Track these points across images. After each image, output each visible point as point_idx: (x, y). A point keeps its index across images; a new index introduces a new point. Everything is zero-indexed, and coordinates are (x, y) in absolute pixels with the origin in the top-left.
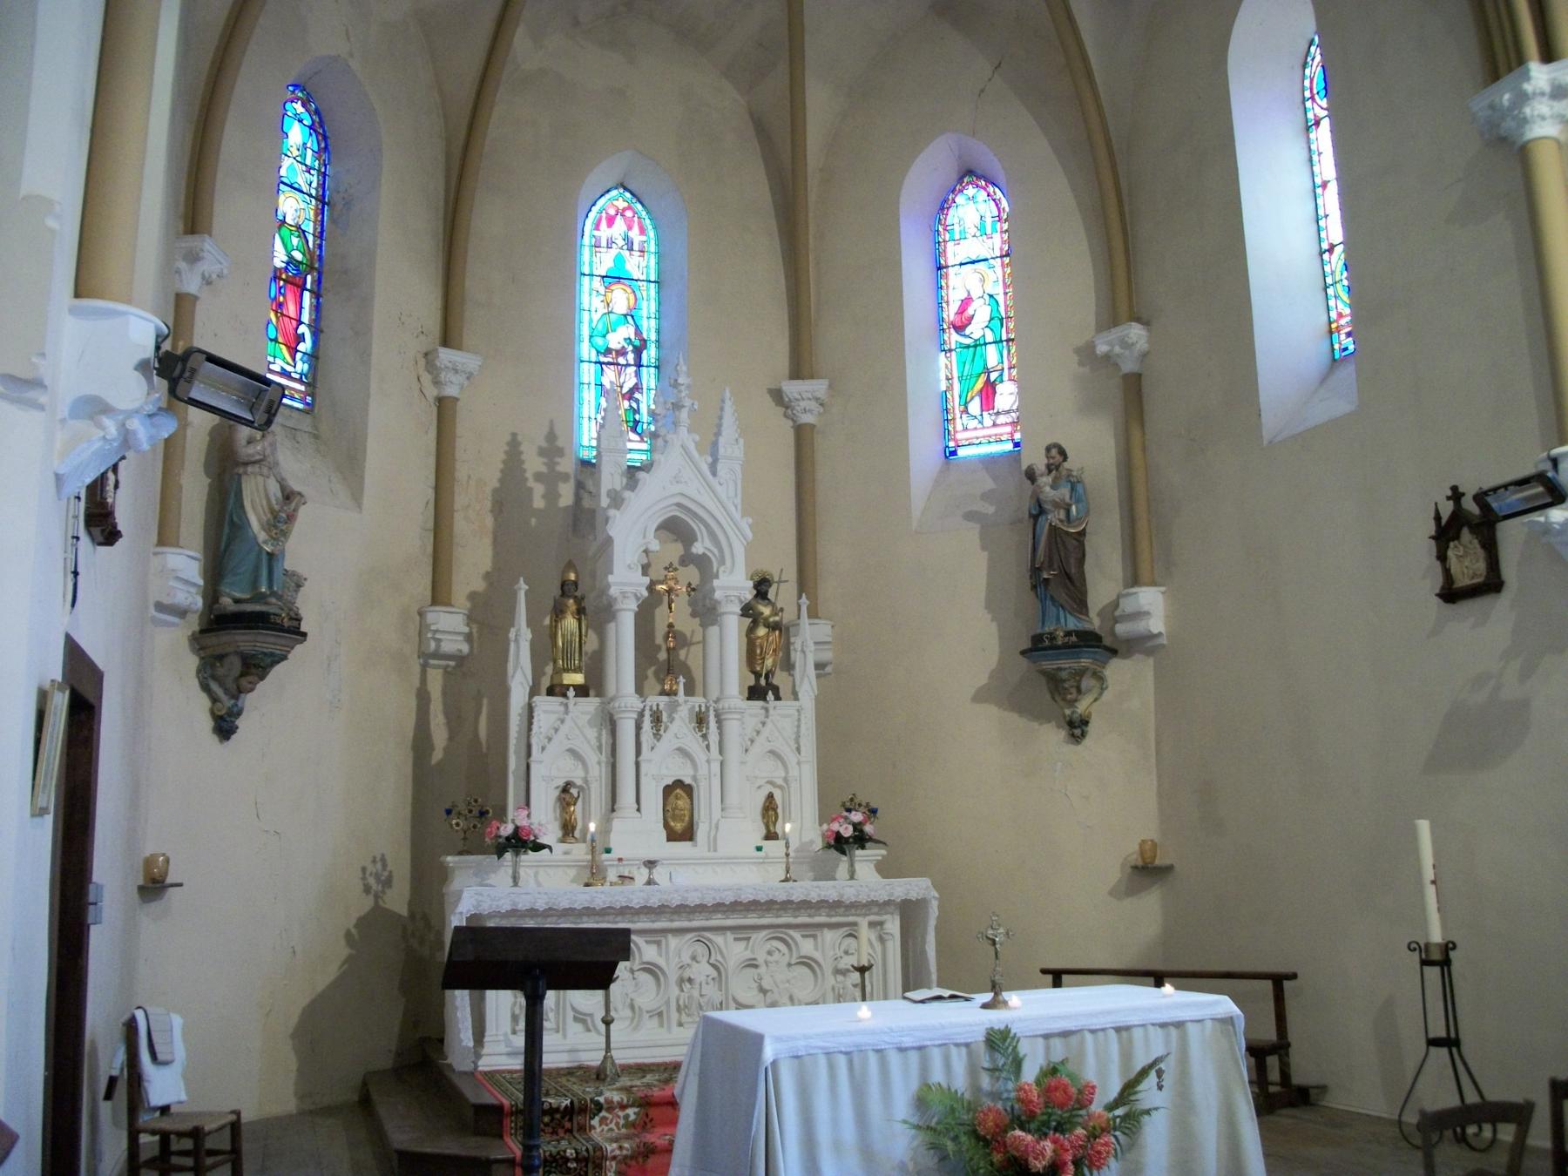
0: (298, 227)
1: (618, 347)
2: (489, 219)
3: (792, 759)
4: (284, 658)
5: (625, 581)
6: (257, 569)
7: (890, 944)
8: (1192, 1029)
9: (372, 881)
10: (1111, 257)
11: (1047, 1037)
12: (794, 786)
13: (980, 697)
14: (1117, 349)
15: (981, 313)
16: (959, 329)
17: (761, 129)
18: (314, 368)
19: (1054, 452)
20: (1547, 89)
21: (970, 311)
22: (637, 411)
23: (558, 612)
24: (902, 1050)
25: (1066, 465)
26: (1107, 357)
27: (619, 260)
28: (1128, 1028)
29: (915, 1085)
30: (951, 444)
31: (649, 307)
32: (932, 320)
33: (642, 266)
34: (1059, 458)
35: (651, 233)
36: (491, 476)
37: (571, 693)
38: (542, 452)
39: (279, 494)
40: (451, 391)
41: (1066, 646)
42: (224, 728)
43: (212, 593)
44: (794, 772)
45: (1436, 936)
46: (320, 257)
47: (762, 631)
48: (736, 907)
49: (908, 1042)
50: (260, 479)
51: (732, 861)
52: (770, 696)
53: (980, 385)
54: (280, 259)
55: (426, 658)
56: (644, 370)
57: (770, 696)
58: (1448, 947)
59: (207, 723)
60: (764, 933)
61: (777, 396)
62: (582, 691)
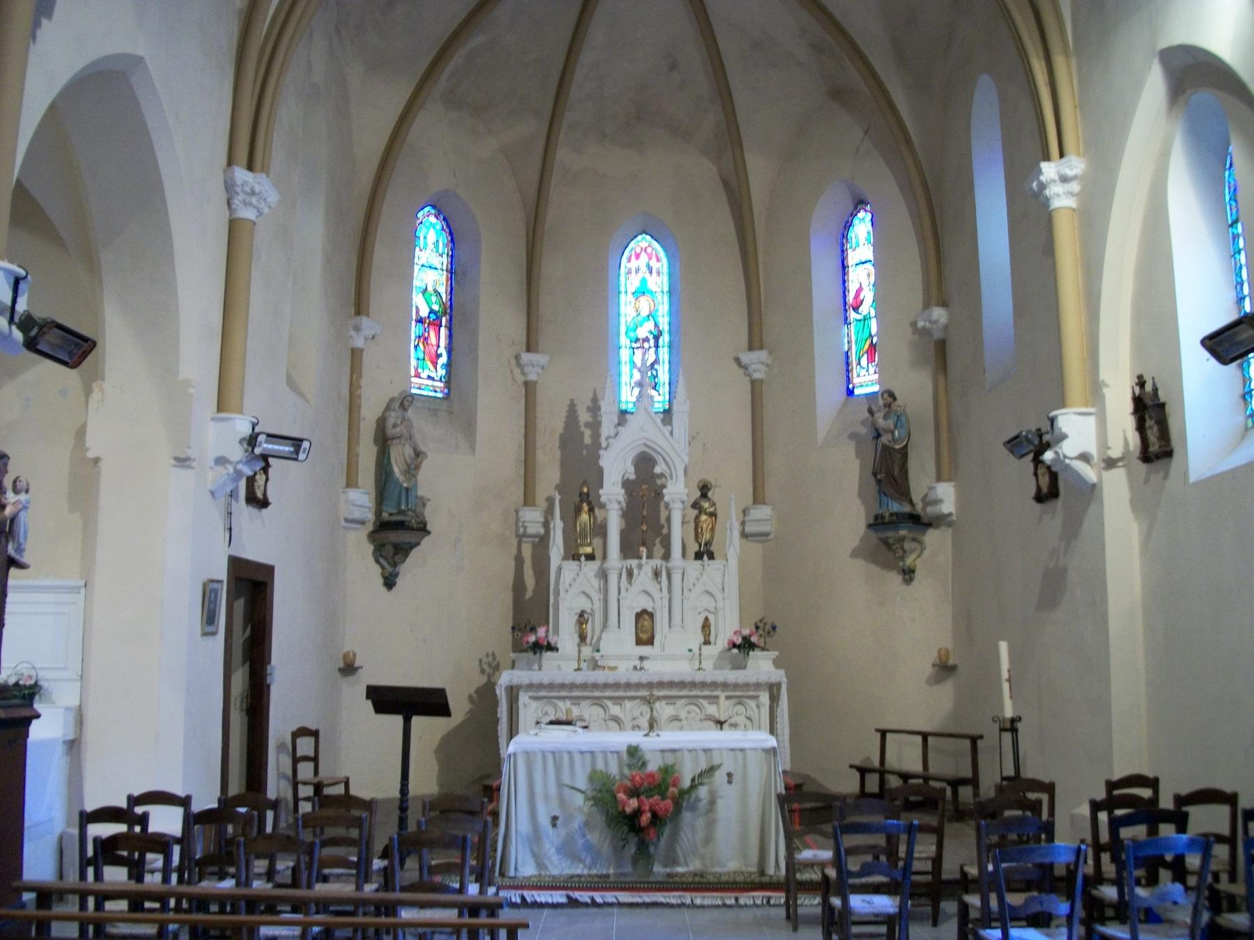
2: (553, 268)
3: (719, 595)
5: (612, 493)
6: (400, 497)
7: (762, 710)
8: (750, 754)
9: (485, 667)
10: (20, 587)
11: (662, 751)
12: (721, 613)
13: (855, 554)
14: (928, 324)
16: (856, 309)
17: (726, 184)
18: (449, 373)
19: (886, 396)
20: (1057, 178)
22: (656, 377)
23: (578, 511)
24: (582, 753)
25: (897, 403)
26: (924, 328)
27: (644, 281)
28: (710, 750)
29: (588, 769)
33: (659, 283)
34: (890, 400)
36: (559, 425)
37: (583, 558)
38: (589, 409)
39: (412, 454)
40: (532, 377)
41: (890, 523)
42: (389, 583)
43: (378, 512)
44: (720, 604)
45: (1009, 713)
47: (704, 517)
48: (671, 684)
49: (584, 748)
51: (673, 658)
52: (705, 557)
53: (867, 347)
54: (424, 313)
55: (520, 537)
56: (660, 350)
57: (705, 557)
58: (1013, 721)
59: (381, 581)
60: (683, 701)
62: (590, 557)
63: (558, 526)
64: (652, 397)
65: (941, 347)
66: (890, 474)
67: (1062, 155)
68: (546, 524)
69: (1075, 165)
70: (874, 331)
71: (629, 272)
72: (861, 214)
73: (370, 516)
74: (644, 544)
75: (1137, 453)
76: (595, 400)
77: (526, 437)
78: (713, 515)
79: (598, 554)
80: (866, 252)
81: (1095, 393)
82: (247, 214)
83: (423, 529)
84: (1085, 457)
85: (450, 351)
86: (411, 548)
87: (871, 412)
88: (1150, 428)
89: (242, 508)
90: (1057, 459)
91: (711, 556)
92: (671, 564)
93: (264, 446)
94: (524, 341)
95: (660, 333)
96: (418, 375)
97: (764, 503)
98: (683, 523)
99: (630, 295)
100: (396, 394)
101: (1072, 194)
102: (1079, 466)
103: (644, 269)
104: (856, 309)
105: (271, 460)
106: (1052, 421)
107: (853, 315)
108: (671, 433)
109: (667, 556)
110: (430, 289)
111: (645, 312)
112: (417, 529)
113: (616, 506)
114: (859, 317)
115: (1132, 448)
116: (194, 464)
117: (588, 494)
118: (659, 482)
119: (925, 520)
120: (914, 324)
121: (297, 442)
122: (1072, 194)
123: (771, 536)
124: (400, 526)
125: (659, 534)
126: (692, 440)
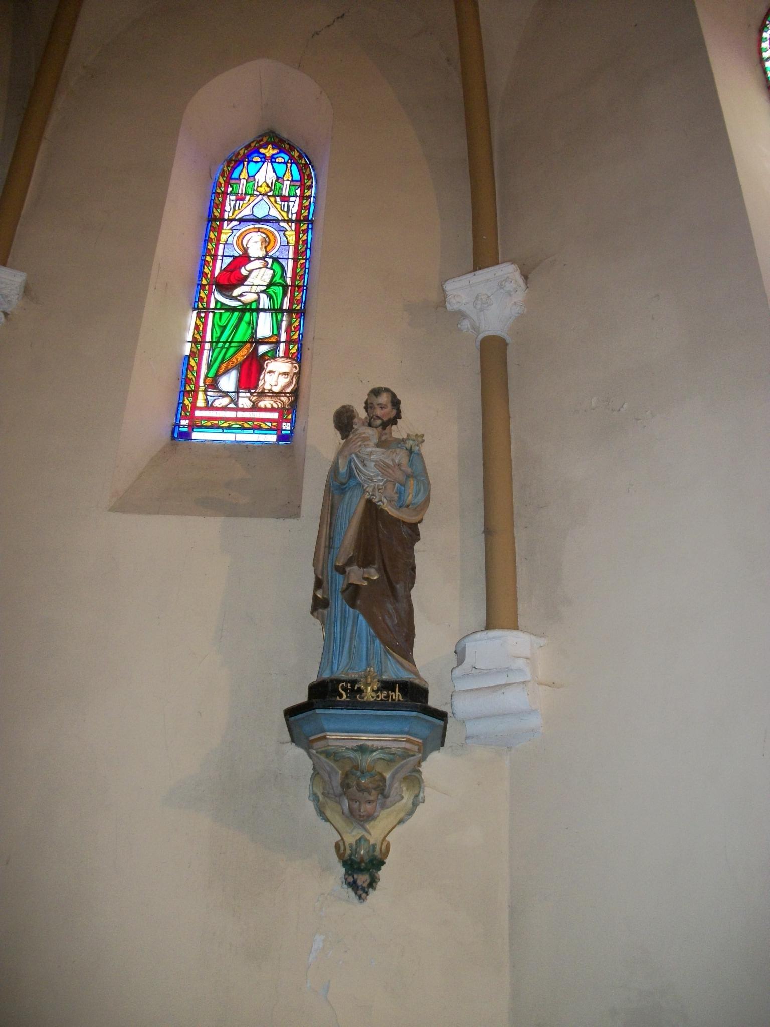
15: (258, 275)
19: (384, 399)
42: (362, 870)
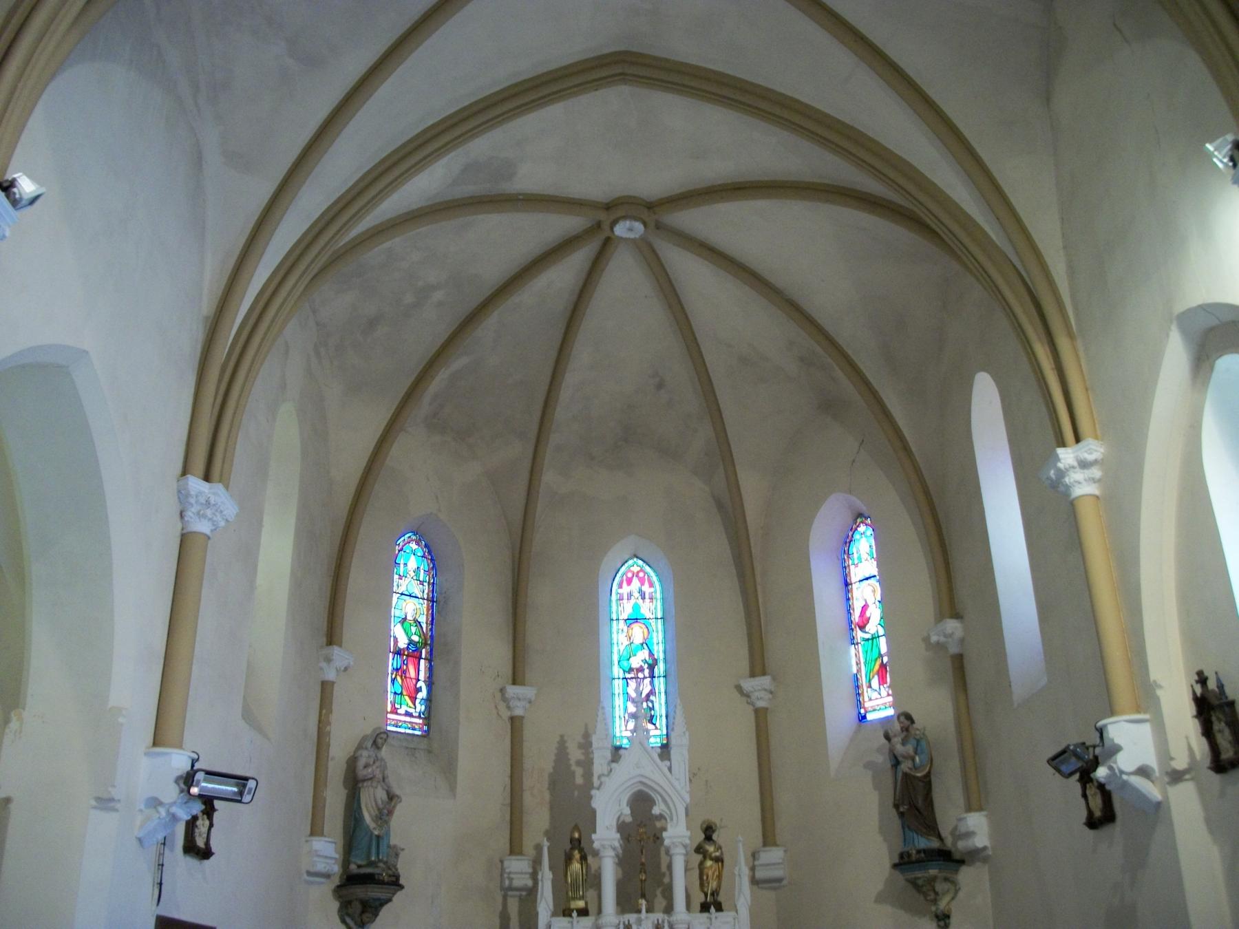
0: (416, 621)
1: (638, 666)
2: (541, 594)
4: (390, 900)
5: (606, 837)
13: (879, 899)
14: (942, 639)
16: (862, 628)
17: (720, 506)
19: (902, 718)
20: (1075, 464)
21: (868, 614)
22: (653, 708)
23: (569, 859)
26: (938, 643)
27: (636, 607)
30: (862, 711)
31: (658, 637)
32: (844, 624)
33: (652, 609)
34: (907, 723)
35: (657, 584)
36: (548, 765)
37: (575, 914)
38: (580, 746)
39: (385, 797)
40: (518, 712)
41: (918, 861)
43: (346, 863)
46: (432, 637)
47: (709, 863)
50: (371, 790)
52: (713, 909)
53: (877, 667)
54: (403, 644)
55: (506, 891)
56: (656, 680)
57: (713, 909)
61: (739, 688)
62: (583, 912)
63: (546, 876)
64: (648, 731)
65: (959, 662)
66: (913, 806)
67: (1078, 439)
68: (534, 875)
69: (1092, 449)
70: (884, 649)
71: (621, 599)
72: (862, 528)
73: (336, 869)
74: (643, 896)
75: (1207, 761)
76: (587, 736)
77: (512, 777)
78: (719, 860)
79: (592, 909)
80: (871, 568)
81: (1146, 700)
82: (202, 527)
83: (395, 883)
84: (1143, 771)
85: (430, 683)
86: (382, 905)
87: (887, 737)
88: (1220, 731)
89: (177, 858)
90: (1115, 774)
91: (719, 908)
92: (674, 918)
93: (204, 785)
94: (510, 673)
95: (656, 662)
96: (395, 711)
97: (775, 844)
98: (686, 870)
99: (622, 622)
100: (369, 731)
101: (1094, 480)
102: (1138, 782)
103: (636, 594)
104: (862, 628)
105: (217, 803)
106: (1101, 732)
107: (859, 635)
108: (670, 769)
109: (669, 909)
110: (409, 617)
111: (638, 639)
112: (388, 884)
113: (612, 853)
114: (868, 636)
115: (1198, 756)
116: (118, 806)
117: (579, 841)
118: (658, 824)
119: (957, 856)
120: (926, 640)
121: (242, 780)
122: (1094, 480)
123: (785, 882)
124: (368, 879)
125: (660, 883)
126: (693, 777)
